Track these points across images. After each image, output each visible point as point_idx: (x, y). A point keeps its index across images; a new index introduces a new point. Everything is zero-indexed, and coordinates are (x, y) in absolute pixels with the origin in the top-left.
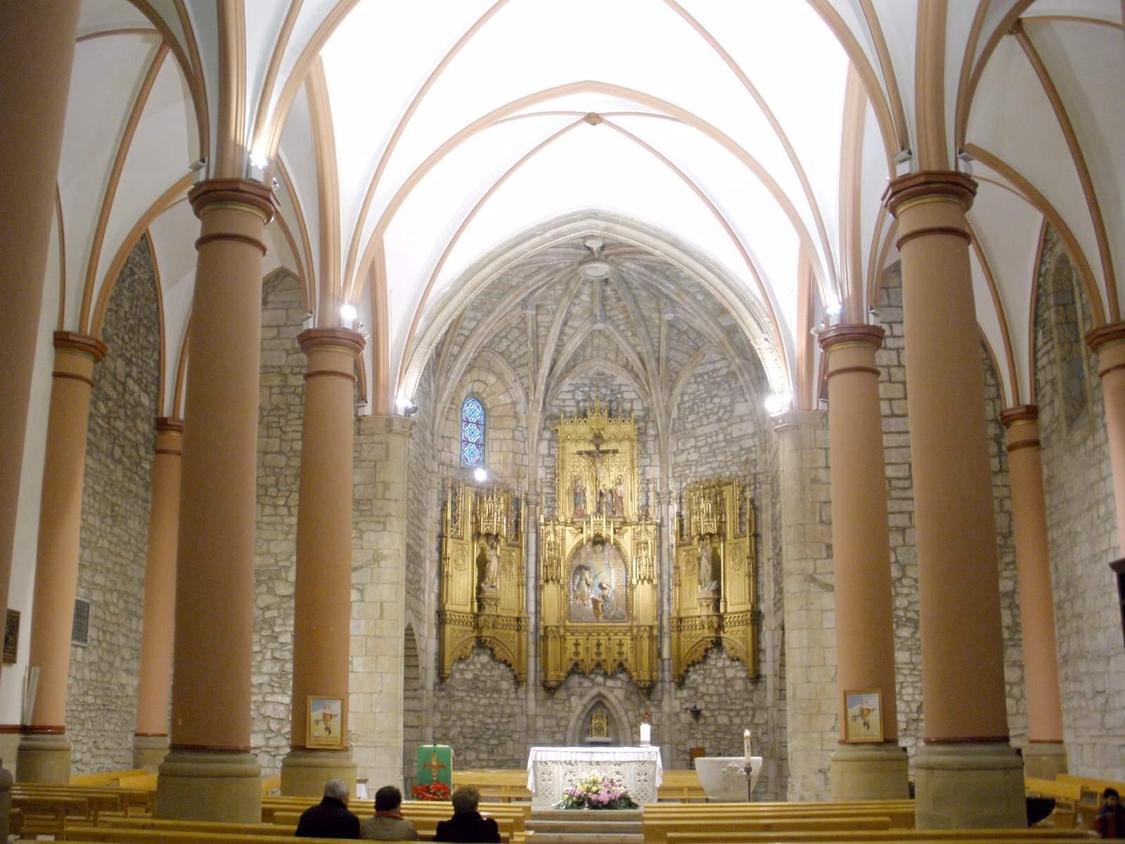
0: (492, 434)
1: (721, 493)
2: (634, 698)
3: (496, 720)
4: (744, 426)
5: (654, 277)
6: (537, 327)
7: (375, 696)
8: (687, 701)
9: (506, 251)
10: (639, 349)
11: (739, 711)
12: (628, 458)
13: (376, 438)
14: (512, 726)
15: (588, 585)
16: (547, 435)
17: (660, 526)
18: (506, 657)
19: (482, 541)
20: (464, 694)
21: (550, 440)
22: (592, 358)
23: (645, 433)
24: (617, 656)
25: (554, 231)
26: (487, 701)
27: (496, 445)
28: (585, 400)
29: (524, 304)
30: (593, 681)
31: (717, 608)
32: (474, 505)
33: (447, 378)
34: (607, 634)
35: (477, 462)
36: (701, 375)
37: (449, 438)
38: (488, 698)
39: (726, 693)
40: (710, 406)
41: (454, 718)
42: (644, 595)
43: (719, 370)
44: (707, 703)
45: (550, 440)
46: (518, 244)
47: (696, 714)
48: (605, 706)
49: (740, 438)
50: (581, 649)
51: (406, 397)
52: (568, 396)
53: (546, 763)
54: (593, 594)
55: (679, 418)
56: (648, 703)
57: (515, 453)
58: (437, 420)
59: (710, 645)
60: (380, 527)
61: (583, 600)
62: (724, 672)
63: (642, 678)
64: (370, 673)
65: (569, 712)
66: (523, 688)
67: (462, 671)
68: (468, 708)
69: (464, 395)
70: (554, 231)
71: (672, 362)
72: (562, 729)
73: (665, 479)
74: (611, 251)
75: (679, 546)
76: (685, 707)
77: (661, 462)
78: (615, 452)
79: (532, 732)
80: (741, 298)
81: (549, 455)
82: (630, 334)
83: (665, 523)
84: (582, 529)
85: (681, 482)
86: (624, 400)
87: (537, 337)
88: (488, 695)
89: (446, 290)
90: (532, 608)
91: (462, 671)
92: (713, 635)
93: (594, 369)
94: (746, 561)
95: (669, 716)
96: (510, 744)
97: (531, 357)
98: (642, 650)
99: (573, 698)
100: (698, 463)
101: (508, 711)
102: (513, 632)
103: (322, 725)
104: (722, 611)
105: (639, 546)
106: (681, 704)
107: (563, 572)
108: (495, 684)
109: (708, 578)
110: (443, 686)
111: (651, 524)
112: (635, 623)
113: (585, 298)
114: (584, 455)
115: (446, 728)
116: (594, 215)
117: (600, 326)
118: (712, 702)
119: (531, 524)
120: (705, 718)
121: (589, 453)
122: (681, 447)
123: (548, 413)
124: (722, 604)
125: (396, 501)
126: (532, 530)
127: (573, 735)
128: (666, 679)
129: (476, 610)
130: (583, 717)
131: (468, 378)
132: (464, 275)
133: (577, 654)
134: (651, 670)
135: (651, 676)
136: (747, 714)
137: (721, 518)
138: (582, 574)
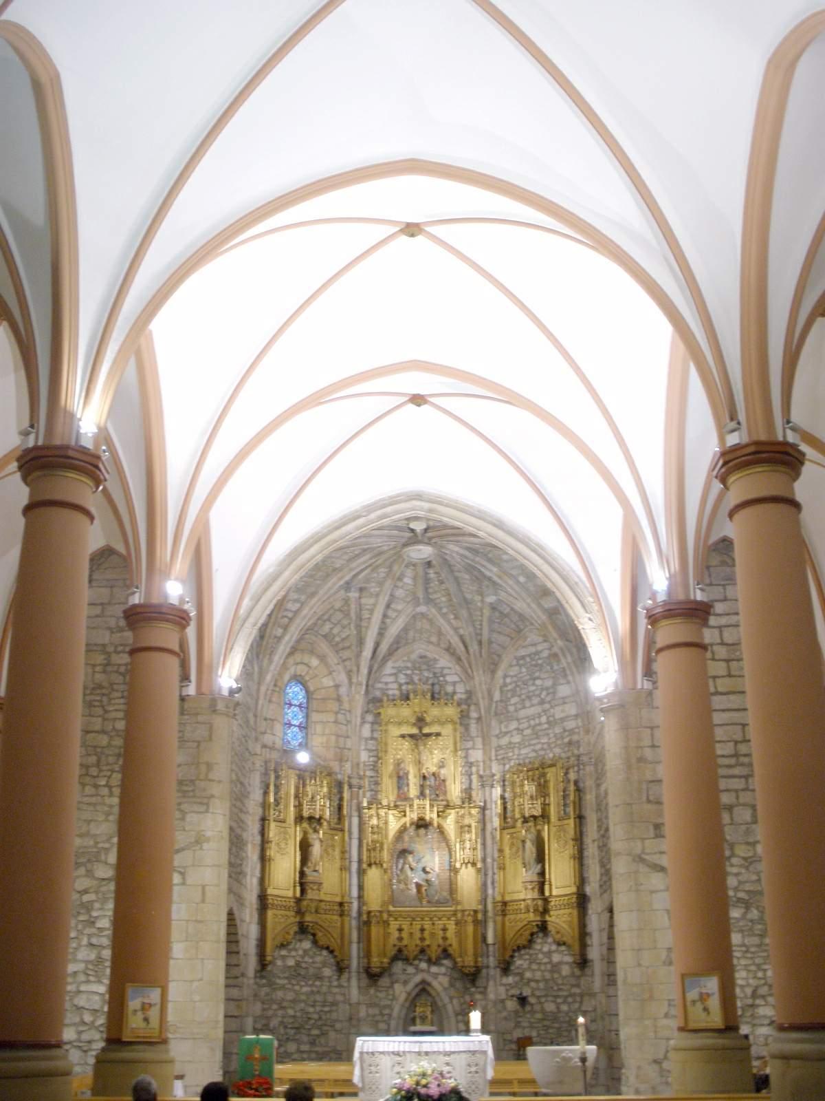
0: (315, 717)
1: (544, 775)
2: (459, 984)
3: (318, 1009)
4: (567, 707)
5: (477, 559)
6: (361, 610)
7: (195, 984)
8: (512, 988)
9: (330, 532)
10: (462, 632)
11: (566, 997)
12: (451, 741)
13: (200, 718)
15: (412, 869)
16: (370, 718)
17: (483, 809)
18: (328, 943)
19: (305, 825)
20: (286, 981)
21: (372, 723)
22: (414, 641)
23: (468, 716)
24: (441, 941)
25: (379, 513)
27: (319, 728)
28: (407, 683)
29: (348, 586)
30: (417, 968)
31: (542, 891)
32: (297, 788)
33: (271, 661)
34: (431, 919)
35: (300, 745)
36: (523, 658)
37: (272, 720)
38: (311, 986)
39: (553, 979)
40: (532, 688)
42: (467, 879)
43: (541, 652)
44: (533, 990)
45: (372, 723)
46: (344, 524)
47: (523, 1000)
48: (429, 994)
49: (563, 720)
50: (405, 935)
51: (230, 677)
52: (390, 679)
53: (373, 1053)
54: (416, 878)
55: (501, 701)
57: (338, 736)
58: (260, 702)
59: (535, 930)
60: (203, 808)
61: (406, 884)
62: (550, 958)
63: (466, 964)
64: (190, 959)
65: (392, 1000)
66: (346, 975)
67: (284, 958)
68: (290, 996)
69: (287, 677)
70: (379, 513)
71: (494, 645)
73: (488, 762)
74: (436, 532)
75: (503, 829)
76: (510, 994)
77: (484, 744)
78: (438, 735)
79: (354, 1022)
80: (566, 579)
81: (372, 738)
82: (452, 617)
83: (488, 806)
84: (405, 812)
85: (504, 765)
86: (447, 682)
87: (361, 620)
88: (310, 982)
89: (271, 570)
90: (355, 893)
91: (284, 958)
92: (538, 918)
93: (417, 652)
94: (571, 843)
95: (495, 1003)
96: (332, 1035)
97: (354, 640)
99: (397, 986)
100: (521, 745)
101: (330, 999)
102: (336, 917)
103: (140, 1015)
104: (547, 893)
105: (463, 829)
106: (507, 990)
107: (385, 855)
109: (532, 861)
110: (264, 973)
111: (474, 807)
112: (459, 907)
113: (407, 580)
114: (407, 738)
115: (267, 1017)
116: (418, 496)
117: (422, 609)
118: (538, 989)
119: (354, 808)
120: (532, 1005)
121: (412, 736)
122: (504, 730)
123: (371, 696)
124: (547, 887)
125: (220, 782)
126: (355, 814)
129: (298, 894)
130: (407, 1004)
131: (291, 660)
132: (289, 555)
133: (400, 939)
134: (476, 955)
135: (476, 962)
136: (575, 1001)
137: (545, 801)
138: (405, 858)
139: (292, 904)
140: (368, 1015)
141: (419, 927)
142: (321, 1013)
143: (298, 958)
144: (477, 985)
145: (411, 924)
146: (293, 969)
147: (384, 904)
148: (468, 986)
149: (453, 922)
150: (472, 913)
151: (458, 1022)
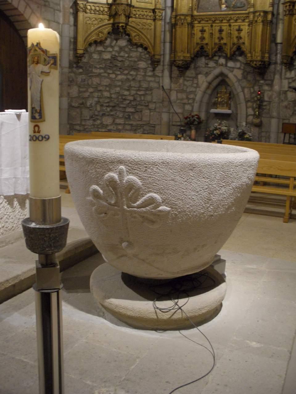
2: (250, 77)
3: (133, 92)
14: (149, 98)
18: (142, 41)
20: (102, 71)
24: (235, 40)
26: (124, 77)
30: (216, 62)
38: (126, 75)
41: (91, 90)
50: (206, 35)
56: (262, 82)
63: (254, 58)
65: (196, 88)
66: (160, 68)
67: (100, 53)
68: (106, 82)
72: (190, 101)
73: (274, 20)
88: (126, 72)
95: (279, 94)
96: (146, 112)
98: (256, 33)
99: (199, 76)
101: (145, 85)
102: (149, 21)
106: (289, 83)
108: (132, 63)
110: (80, 64)
115: (83, 98)
127: (200, 106)
128: (279, 61)
130: (209, 92)
133: (203, 38)
134: (263, 52)
135: (263, 57)
139: (106, 10)
140: (177, 99)
141: (218, 28)
142: (136, 96)
143: (114, 53)
144: (265, 78)
145: (212, 26)
146: (109, 62)
147: (191, 9)
148: (258, 78)
149: (247, 24)
150: (262, 14)
151: (247, 108)
